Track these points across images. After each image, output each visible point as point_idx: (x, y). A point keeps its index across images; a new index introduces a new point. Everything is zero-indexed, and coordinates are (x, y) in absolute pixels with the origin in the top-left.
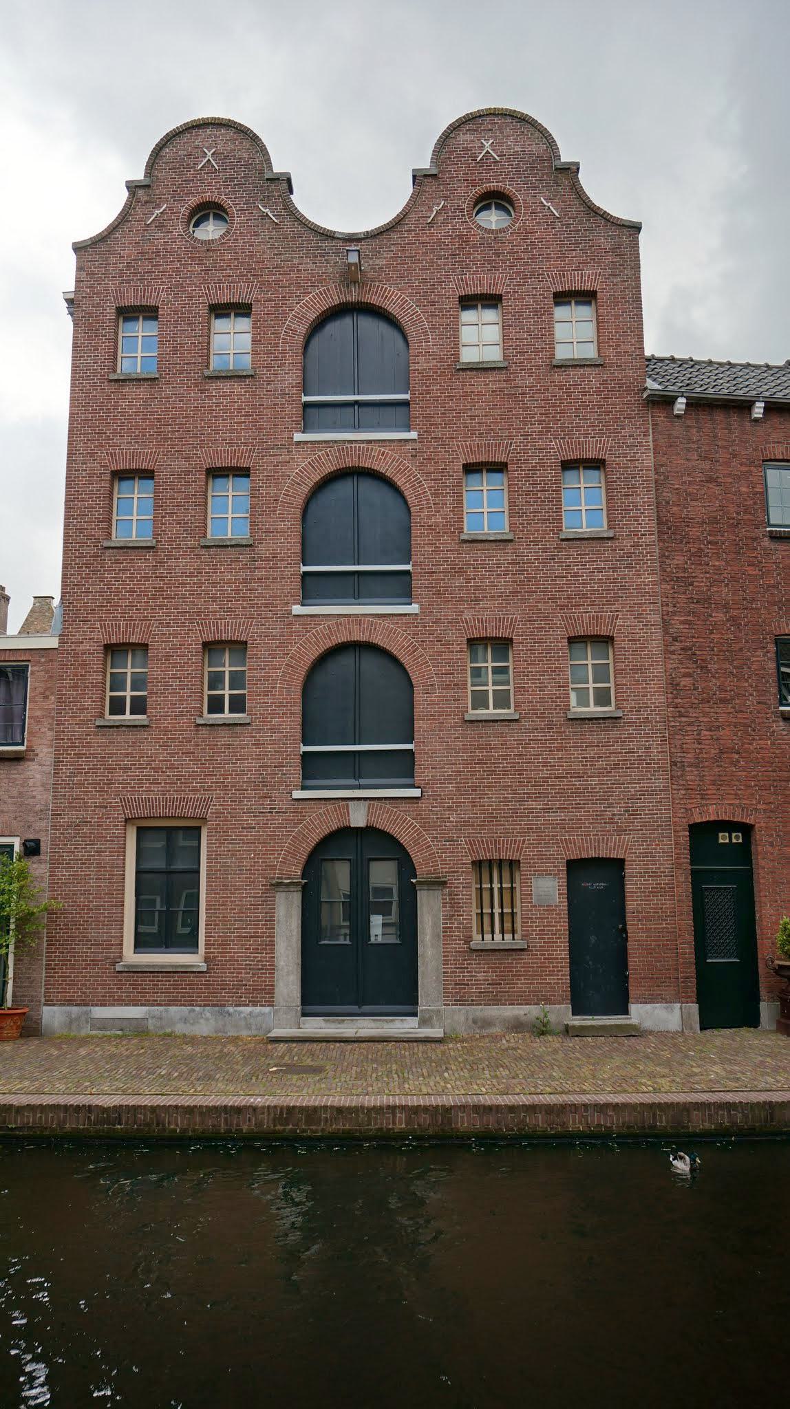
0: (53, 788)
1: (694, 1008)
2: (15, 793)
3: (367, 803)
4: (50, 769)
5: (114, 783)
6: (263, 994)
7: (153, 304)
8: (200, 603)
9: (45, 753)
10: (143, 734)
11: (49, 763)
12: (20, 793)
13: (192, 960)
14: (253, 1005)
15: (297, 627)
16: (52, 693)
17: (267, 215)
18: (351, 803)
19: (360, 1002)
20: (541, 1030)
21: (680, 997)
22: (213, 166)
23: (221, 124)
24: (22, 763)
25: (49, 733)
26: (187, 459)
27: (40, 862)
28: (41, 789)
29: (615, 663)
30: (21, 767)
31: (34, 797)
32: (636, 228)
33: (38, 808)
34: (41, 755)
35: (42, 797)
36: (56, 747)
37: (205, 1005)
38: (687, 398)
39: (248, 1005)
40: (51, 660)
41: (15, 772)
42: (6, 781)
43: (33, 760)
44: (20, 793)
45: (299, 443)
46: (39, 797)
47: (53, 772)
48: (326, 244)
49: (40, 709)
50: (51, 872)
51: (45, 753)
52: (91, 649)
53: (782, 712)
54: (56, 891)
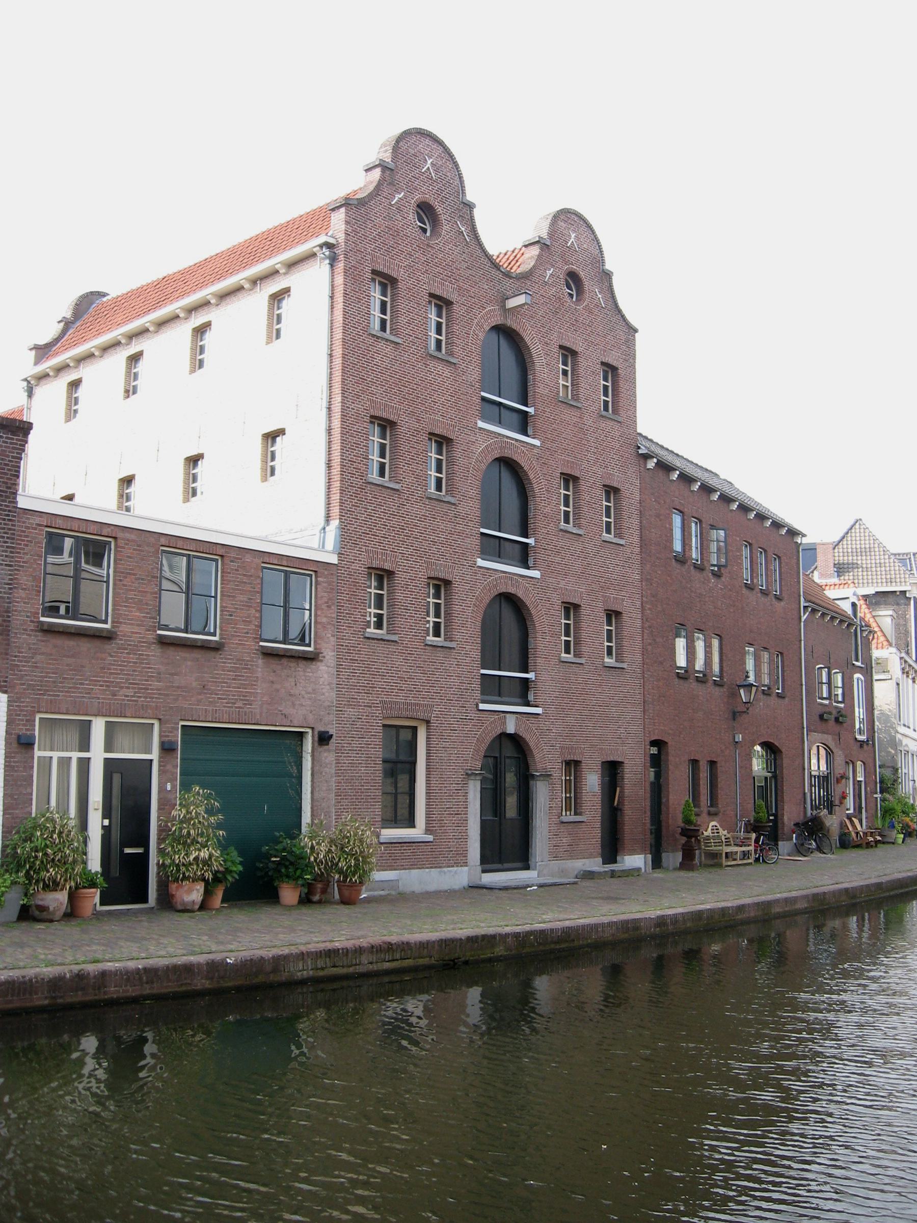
0: (337, 688)
1: (649, 857)
2: (310, 689)
3: (515, 716)
4: (334, 671)
5: (376, 687)
6: (460, 859)
7: (395, 276)
8: (425, 544)
9: (329, 655)
10: (392, 648)
11: (332, 665)
12: (314, 690)
13: (417, 832)
14: (457, 866)
15: (479, 576)
16: (333, 604)
17: (462, 232)
18: (508, 715)
19: (500, 861)
20: (589, 875)
21: (642, 851)
22: (430, 174)
23: (436, 140)
24: (314, 663)
25: (332, 639)
26: (418, 421)
27: (329, 751)
28: (328, 687)
29: (616, 629)
30: (313, 666)
31: (323, 694)
32: (636, 331)
33: (327, 704)
34: (327, 657)
35: (329, 695)
36: (337, 652)
37: (431, 868)
38: (658, 460)
39: (453, 866)
40: (332, 574)
41: (309, 670)
42: (303, 678)
43: (322, 661)
44: (314, 690)
45: (480, 429)
46: (327, 694)
47: (336, 673)
48: (494, 271)
49: (325, 617)
50: (336, 760)
51: (329, 655)
52: (359, 567)
53: (42, 623)
54: (340, 776)
